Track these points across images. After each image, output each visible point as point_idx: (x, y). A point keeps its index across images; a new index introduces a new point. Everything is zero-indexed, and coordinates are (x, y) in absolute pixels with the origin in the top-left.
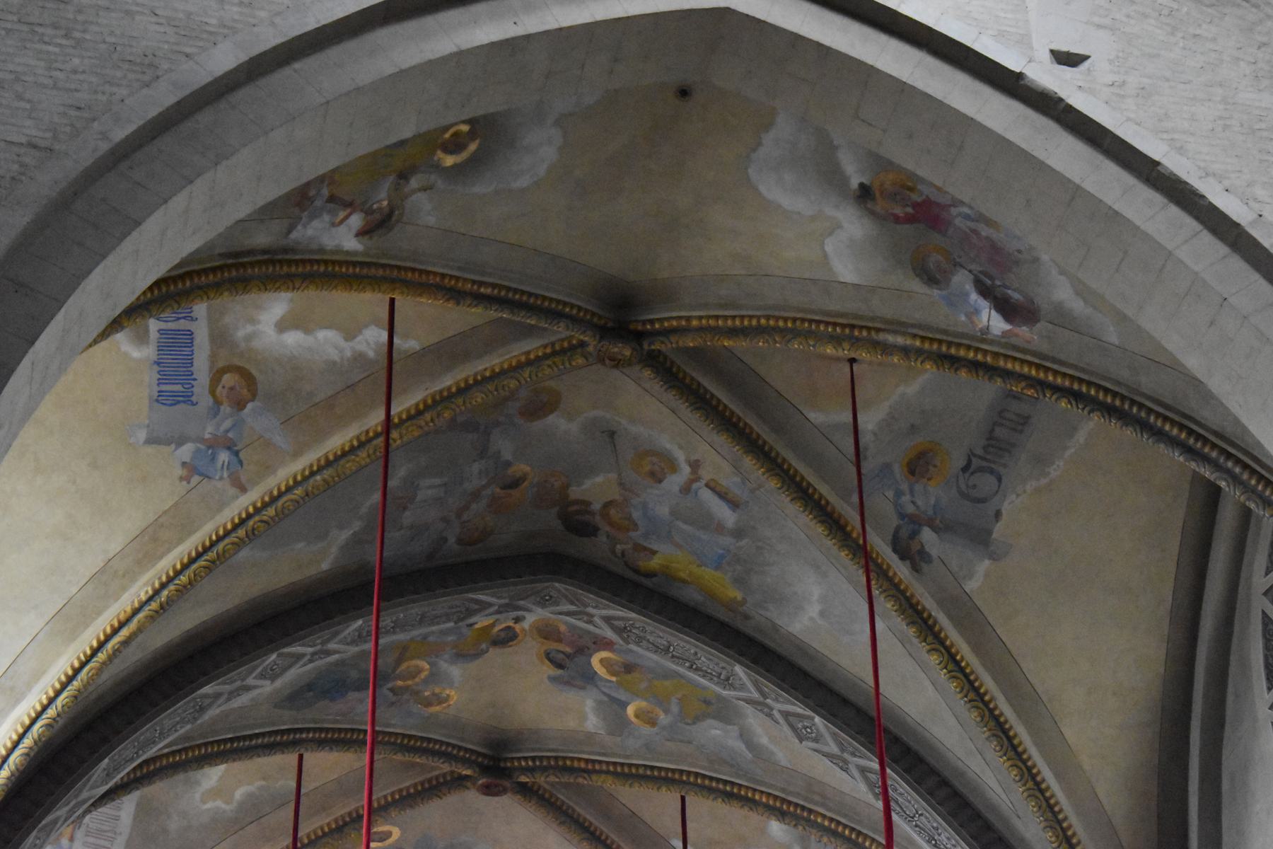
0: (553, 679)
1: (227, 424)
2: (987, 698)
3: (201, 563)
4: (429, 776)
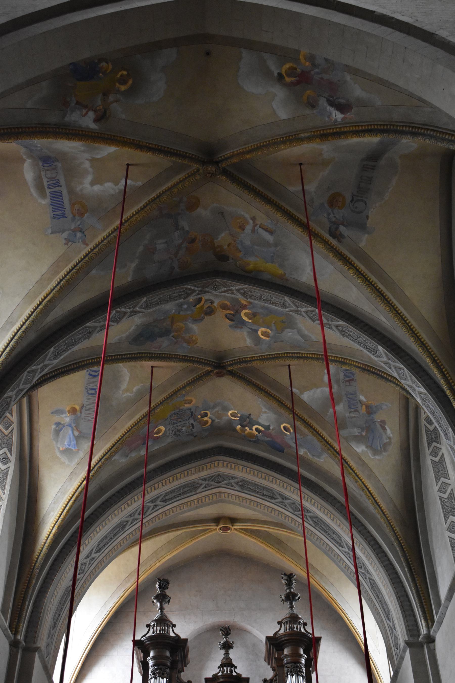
0: (230, 326)
1: (79, 223)
2: (373, 283)
3: (74, 271)
4: (198, 374)
